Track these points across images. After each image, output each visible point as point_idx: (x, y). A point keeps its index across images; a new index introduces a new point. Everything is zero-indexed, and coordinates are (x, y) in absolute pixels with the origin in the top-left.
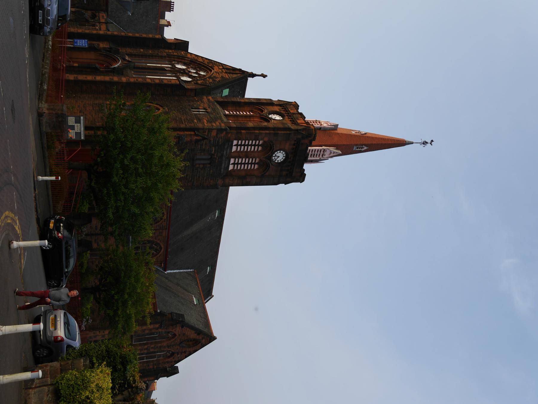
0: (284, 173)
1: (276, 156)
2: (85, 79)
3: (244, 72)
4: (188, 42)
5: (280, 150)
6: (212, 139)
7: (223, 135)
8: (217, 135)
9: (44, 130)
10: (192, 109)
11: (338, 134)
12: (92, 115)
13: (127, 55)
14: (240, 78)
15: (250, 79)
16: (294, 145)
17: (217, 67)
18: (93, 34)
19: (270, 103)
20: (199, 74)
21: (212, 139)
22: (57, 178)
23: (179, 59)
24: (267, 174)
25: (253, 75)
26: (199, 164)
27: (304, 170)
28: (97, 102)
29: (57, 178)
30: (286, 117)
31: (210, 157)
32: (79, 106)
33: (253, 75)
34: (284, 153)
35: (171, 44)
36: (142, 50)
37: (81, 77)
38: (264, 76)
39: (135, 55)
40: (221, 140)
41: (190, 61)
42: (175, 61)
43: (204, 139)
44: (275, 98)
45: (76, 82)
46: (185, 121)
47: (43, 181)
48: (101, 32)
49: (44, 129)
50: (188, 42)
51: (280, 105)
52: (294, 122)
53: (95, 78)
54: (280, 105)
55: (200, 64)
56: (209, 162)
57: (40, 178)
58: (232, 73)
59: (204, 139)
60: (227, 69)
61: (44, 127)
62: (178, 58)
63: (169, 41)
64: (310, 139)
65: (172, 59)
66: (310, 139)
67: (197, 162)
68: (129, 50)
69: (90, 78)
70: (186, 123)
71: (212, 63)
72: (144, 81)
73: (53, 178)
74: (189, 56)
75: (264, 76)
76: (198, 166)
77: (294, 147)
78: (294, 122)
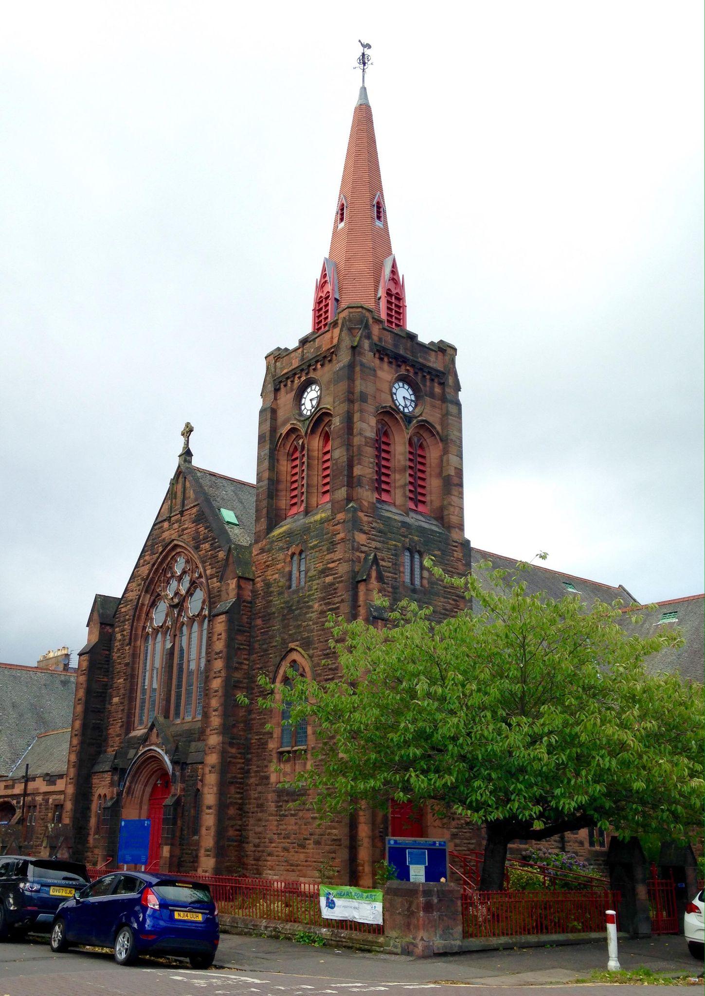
0: (437, 390)
1: (406, 406)
2: (212, 832)
3: (179, 473)
4: (98, 597)
5: (392, 394)
6: (374, 544)
7: (365, 519)
8: (365, 533)
9: (458, 943)
10: (290, 587)
11: (348, 260)
12: (314, 818)
13: (128, 731)
14: (191, 491)
15: (196, 462)
16: (381, 359)
17: (166, 535)
18: (75, 810)
19: (269, 414)
20: (184, 572)
21: (374, 544)
22: (610, 919)
23: (139, 616)
24: (439, 428)
25: (187, 454)
26: (422, 578)
27: (432, 343)
28: (272, 807)
29: (610, 919)
30: (312, 375)
31: (407, 554)
32: (286, 849)
33: (187, 454)
34: (396, 386)
35: (102, 634)
36: (116, 700)
37: (207, 839)
38: (188, 431)
39: (130, 715)
40: (374, 525)
41: (147, 592)
42: (144, 628)
43: (375, 560)
44: (259, 403)
45: (220, 851)
46: (329, 604)
47: (620, 959)
48: (70, 790)
49: (457, 943)
50: (98, 597)
51: (277, 390)
52: (325, 358)
53: (209, 808)
54: (277, 390)
55: (157, 570)
56: (417, 556)
57: (613, 964)
58: (184, 498)
59: (375, 560)
60: (171, 510)
61: (453, 942)
62: (139, 619)
63: (95, 639)
64: (371, 321)
65: (139, 635)
66: (371, 321)
67: (417, 582)
68: (115, 729)
69: (209, 820)
70: (337, 600)
71: (153, 545)
72: (220, 693)
73: (612, 928)
74: (132, 595)
75: (188, 431)
76: (425, 582)
77: (386, 359)
78: (325, 358)
